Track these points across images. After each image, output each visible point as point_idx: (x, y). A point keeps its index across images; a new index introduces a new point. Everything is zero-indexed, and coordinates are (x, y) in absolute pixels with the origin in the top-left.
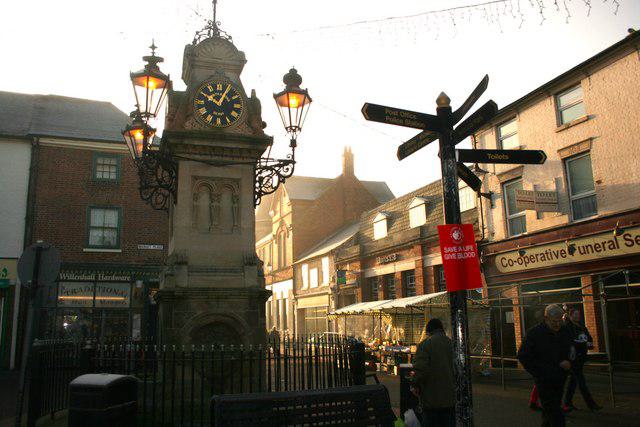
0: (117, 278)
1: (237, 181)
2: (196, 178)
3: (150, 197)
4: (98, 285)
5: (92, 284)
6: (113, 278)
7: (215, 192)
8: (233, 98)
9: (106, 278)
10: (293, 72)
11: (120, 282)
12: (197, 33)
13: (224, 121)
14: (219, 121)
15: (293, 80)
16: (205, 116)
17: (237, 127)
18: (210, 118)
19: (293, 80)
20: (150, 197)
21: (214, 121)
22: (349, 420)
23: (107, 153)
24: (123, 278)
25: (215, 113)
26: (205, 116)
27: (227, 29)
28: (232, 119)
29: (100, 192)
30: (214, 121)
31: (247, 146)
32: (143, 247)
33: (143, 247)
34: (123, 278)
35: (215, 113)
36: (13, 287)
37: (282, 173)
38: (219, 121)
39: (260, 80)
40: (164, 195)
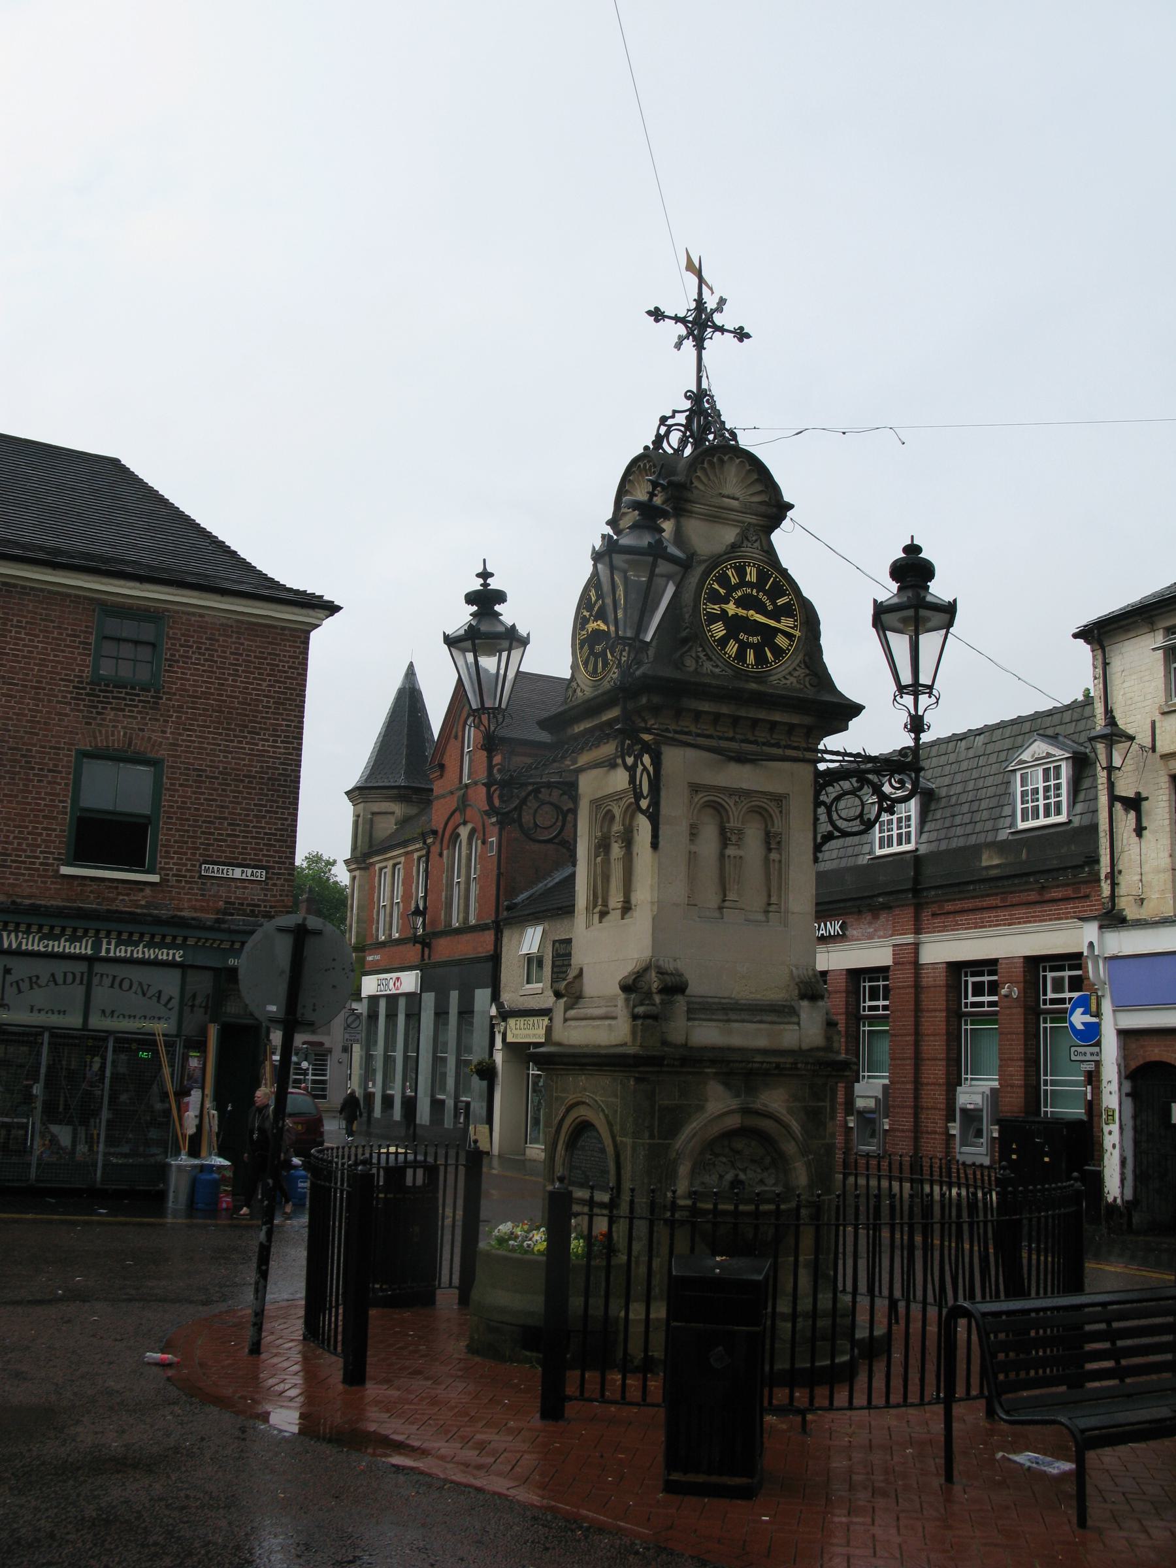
0: (150, 954)
1: (779, 799)
2: (695, 788)
3: (519, 809)
4: (99, 968)
5: (82, 967)
6: (139, 952)
7: (733, 824)
8: (780, 602)
9: (122, 952)
10: (912, 549)
11: (156, 963)
12: (663, 420)
13: (761, 659)
14: (751, 657)
15: (912, 570)
16: (723, 642)
17: (784, 674)
18: (732, 648)
19: (912, 570)
20: (519, 809)
21: (741, 656)
22: (1012, 1354)
23: (147, 609)
24: (163, 955)
25: (742, 636)
26: (723, 642)
27: (739, 415)
28: (778, 652)
29: (111, 715)
30: (741, 656)
31: (795, 719)
32: (214, 871)
33: (214, 871)
34: (163, 955)
35: (742, 636)
36: (1114, 1111)
37: (887, 789)
38: (751, 657)
39: (832, 564)
40: (557, 808)
